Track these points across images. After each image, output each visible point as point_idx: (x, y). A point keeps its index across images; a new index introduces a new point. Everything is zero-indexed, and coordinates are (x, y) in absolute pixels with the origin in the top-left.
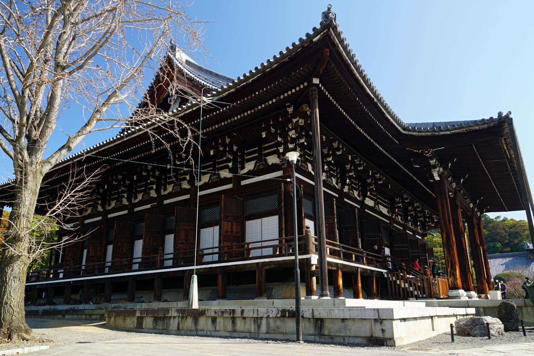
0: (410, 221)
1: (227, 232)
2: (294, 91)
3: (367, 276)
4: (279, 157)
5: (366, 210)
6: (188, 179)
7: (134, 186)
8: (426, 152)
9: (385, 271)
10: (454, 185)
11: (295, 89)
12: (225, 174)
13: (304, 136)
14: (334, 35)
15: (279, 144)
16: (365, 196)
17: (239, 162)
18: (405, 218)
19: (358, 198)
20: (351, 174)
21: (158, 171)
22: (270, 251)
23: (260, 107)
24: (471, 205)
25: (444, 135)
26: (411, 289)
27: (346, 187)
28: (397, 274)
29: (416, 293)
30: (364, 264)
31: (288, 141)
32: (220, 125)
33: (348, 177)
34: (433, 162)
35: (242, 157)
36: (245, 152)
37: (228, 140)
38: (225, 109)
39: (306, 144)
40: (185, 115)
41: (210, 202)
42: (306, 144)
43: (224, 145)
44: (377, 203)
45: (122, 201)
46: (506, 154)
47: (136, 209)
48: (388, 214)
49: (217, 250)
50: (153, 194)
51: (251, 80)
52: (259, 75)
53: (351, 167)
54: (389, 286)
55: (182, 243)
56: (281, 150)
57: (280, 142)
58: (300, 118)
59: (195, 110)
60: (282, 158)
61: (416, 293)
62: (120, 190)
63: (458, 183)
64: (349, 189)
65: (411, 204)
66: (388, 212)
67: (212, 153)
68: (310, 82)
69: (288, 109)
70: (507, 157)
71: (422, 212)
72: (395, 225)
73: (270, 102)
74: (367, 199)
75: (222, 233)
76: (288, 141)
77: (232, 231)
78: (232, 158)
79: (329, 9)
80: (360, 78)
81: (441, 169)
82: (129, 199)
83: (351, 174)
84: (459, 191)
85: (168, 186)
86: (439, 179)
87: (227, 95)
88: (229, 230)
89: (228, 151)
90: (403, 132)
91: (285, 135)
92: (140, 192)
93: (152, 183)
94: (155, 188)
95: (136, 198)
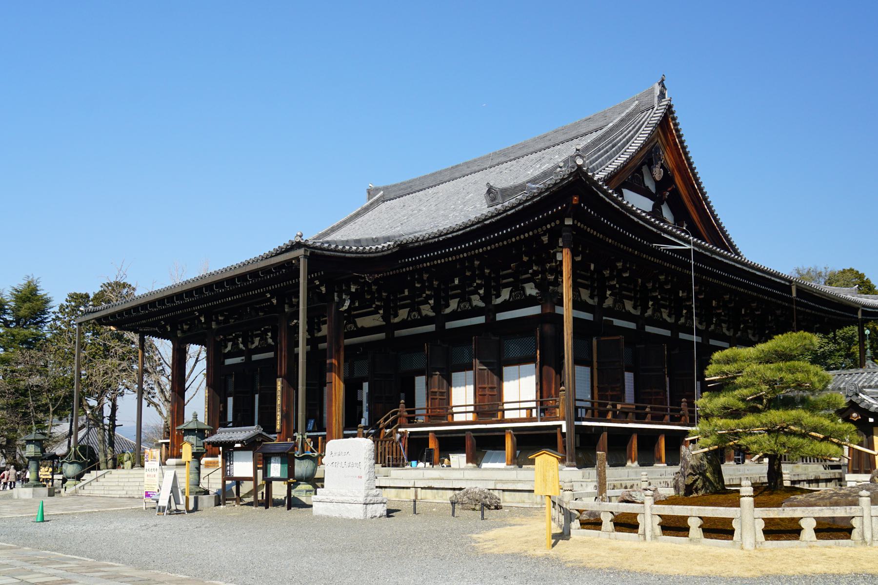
21: (488, 268)
22: (523, 414)
92: (506, 286)
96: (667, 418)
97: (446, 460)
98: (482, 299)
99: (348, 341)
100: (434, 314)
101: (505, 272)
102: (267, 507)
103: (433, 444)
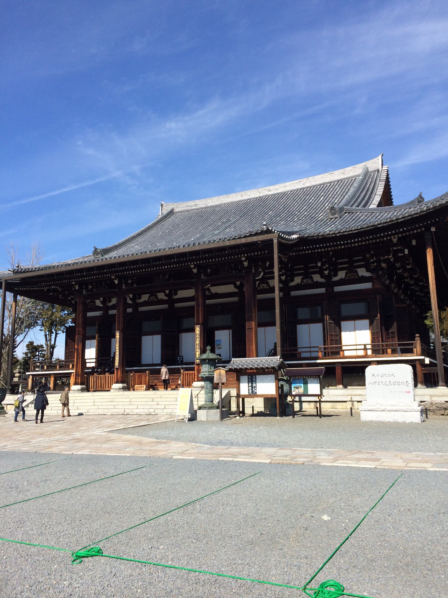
12: (161, 296)
96: (389, 351)
97: (67, 389)
99: (259, 297)
100: (132, 302)
102: (320, 418)
103: (339, 371)
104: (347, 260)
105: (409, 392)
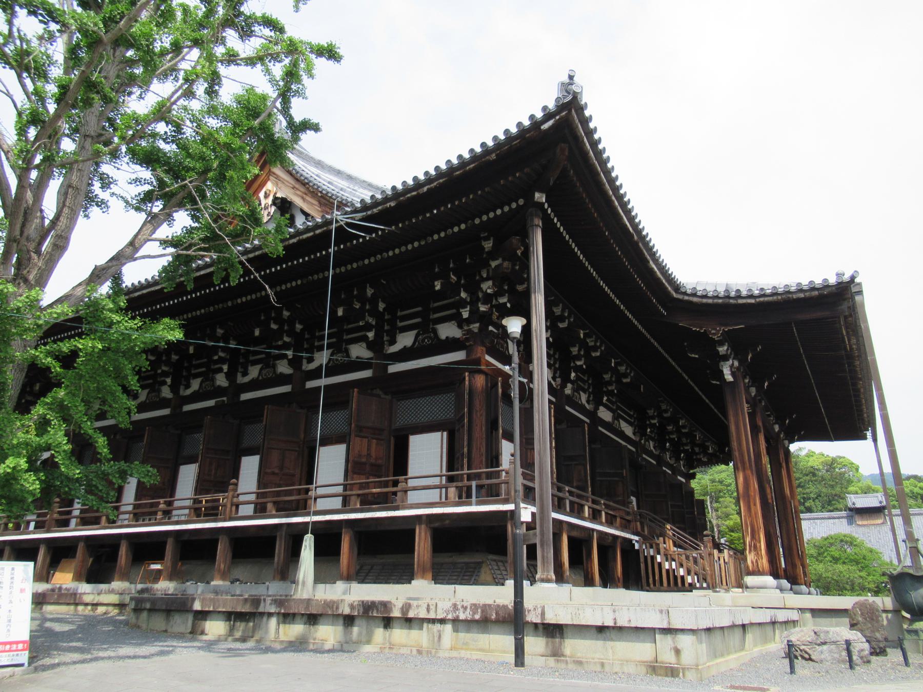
0: (668, 450)
1: (360, 456)
2: (499, 212)
3: (607, 546)
4: (460, 326)
5: (600, 428)
6: (290, 357)
7: (186, 365)
8: (713, 332)
9: (637, 538)
10: (753, 391)
11: (502, 209)
13: (506, 291)
14: (577, 121)
15: (462, 304)
16: (598, 403)
17: (387, 331)
18: (661, 445)
19: (587, 405)
20: (579, 363)
21: (300, 323)
23: (436, 237)
24: (777, 428)
25: (744, 304)
26: (682, 572)
27: (569, 386)
28: (658, 545)
29: (689, 579)
30: (601, 523)
31: (478, 300)
32: (360, 263)
33: (573, 367)
34: (723, 350)
35: (392, 323)
36: (399, 314)
37: (370, 292)
38: (374, 235)
39: (509, 305)
40: (299, 241)
41: (337, 398)
42: (509, 305)
43: (363, 299)
44: (617, 417)
45: (159, 391)
46: (844, 342)
47: (187, 408)
48: (633, 437)
49: (340, 489)
50: (221, 380)
51: (425, 189)
52: (441, 181)
53: (579, 350)
54: (642, 566)
55: (274, 473)
56: (465, 315)
57: (465, 300)
58: (504, 260)
59: (320, 234)
60: (466, 328)
61: (689, 579)
62: (159, 371)
63: (760, 389)
64: (574, 390)
65: (674, 420)
66: (634, 434)
67: (257, 333)
68: (529, 197)
69: (483, 243)
70: (845, 348)
71: (690, 435)
72: (644, 456)
73: (456, 229)
74: (601, 408)
75: (351, 458)
76: (478, 300)
77: (369, 455)
78: (374, 323)
79: (571, 78)
80: (613, 198)
81: (736, 364)
82: (174, 388)
83: (579, 363)
84: (760, 401)
85: (250, 368)
86: (732, 379)
87: (381, 212)
88: (365, 452)
89: (368, 311)
90: (675, 295)
91: (473, 288)
92: (196, 376)
93: (222, 361)
94: (225, 370)
95: (188, 386)
98: (370, 346)
101: (350, 326)
104: (419, 309)
105: (13, 569)
